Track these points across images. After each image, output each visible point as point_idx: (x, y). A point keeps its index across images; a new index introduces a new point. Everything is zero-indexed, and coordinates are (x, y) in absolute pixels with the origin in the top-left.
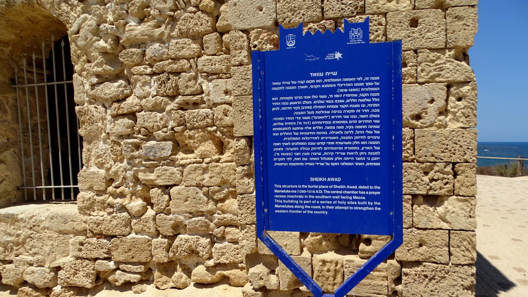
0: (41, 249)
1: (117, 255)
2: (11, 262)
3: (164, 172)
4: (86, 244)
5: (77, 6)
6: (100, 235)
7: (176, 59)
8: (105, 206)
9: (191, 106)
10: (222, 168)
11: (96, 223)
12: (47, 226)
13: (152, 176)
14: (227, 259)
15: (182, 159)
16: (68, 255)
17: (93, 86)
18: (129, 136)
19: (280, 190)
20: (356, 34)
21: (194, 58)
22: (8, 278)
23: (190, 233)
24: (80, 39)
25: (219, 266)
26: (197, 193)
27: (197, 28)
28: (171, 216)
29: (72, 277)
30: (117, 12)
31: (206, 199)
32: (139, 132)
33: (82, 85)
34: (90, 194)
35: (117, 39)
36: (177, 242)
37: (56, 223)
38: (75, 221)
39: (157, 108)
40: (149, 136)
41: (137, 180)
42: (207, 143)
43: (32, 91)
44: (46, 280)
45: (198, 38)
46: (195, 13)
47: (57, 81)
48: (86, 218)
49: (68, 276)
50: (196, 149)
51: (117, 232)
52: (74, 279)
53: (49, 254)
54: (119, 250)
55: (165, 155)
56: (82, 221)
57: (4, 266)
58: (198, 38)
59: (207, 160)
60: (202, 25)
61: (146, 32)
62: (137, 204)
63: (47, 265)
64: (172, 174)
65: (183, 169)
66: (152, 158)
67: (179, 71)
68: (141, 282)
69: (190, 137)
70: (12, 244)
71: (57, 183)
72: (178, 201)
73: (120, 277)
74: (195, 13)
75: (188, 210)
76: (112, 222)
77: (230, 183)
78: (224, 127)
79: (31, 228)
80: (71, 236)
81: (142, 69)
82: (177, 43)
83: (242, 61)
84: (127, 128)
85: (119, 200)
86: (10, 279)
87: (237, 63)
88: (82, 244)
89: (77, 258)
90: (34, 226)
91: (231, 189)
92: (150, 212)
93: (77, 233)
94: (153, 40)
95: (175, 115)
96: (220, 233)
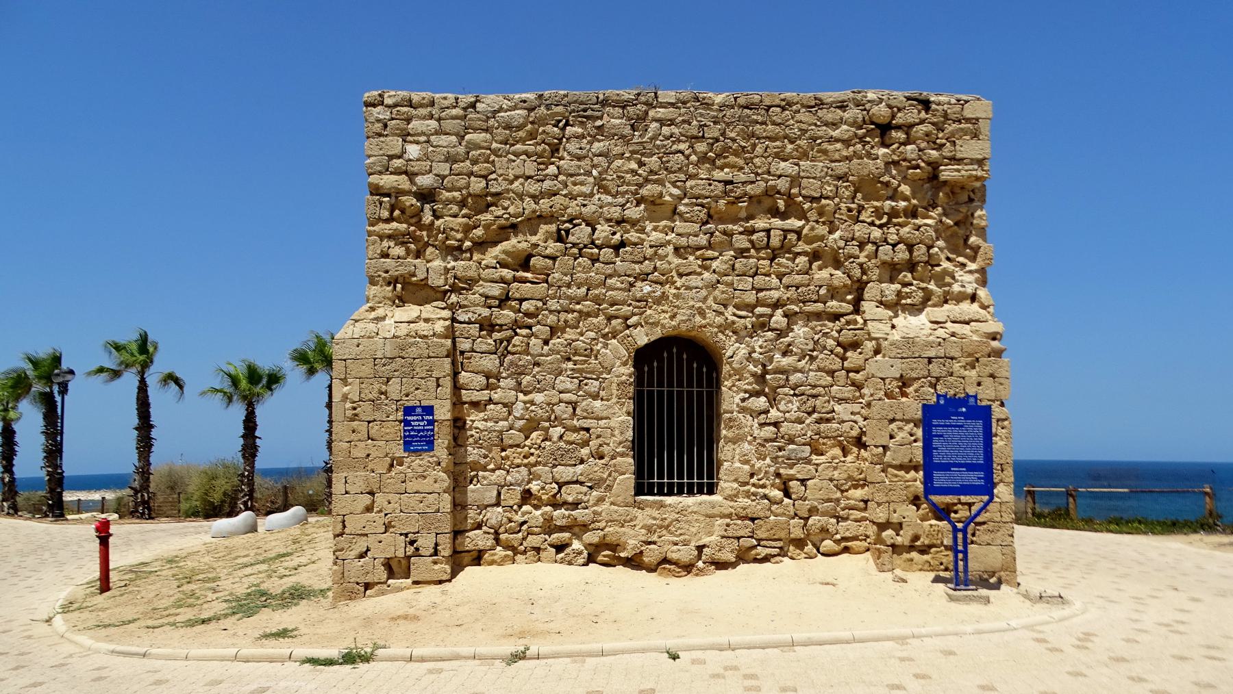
7: (815, 386)
13: (792, 472)
18: (774, 440)
19: (936, 474)
20: (972, 400)
40: (791, 441)
41: (778, 475)
73: (762, 552)
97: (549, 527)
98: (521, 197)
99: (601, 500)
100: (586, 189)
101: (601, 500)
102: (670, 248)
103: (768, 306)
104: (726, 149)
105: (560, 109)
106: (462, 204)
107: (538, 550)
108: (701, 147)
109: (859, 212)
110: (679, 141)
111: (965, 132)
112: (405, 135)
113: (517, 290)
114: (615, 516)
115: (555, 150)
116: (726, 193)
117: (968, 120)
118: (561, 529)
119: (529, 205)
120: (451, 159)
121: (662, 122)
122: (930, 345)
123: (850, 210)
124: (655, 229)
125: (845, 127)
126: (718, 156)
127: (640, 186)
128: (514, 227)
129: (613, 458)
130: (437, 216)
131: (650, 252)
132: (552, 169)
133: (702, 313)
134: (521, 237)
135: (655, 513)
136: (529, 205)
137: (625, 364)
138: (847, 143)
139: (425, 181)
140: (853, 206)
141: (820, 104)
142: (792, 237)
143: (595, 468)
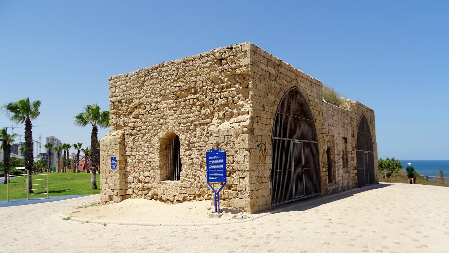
1: (188, 193)
6: (185, 188)
7: (201, 147)
13: (196, 174)
18: (191, 164)
19: (210, 175)
20: (220, 150)
33: (182, 151)
34: (183, 178)
35: (190, 141)
39: (197, 158)
40: (196, 164)
41: (193, 175)
43: (170, 150)
58: (205, 142)
62: (193, 180)
68: (193, 199)
71: (175, 175)
73: (189, 198)
92: (196, 182)
95: (201, 160)
97: (143, 189)
98: (136, 99)
99: (153, 182)
100: (149, 94)
101: (153, 182)
102: (167, 108)
103: (190, 123)
104: (179, 76)
105: (143, 73)
106: (126, 102)
107: (141, 195)
108: (173, 77)
109: (213, 89)
110: (169, 76)
111: (242, 56)
112: (116, 87)
113: (137, 124)
114: (156, 186)
115: (143, 84)
116: (180, 90)
117: (243, 52)
118: (145, 190)
119: (138, 101)
120: (123, 91)
121: (165, 72)
122: (224, 131)
123: (210, 89)
124: (165, 103)
125: (208, 63)
126: (178, 79)
127: (161, 91)
128: (136, 107)
129: (156, 170)
130: (122, 107)
131: (163, 110)
132: (143, 90)
133: (175, 127)
134: (137, 110)
135: (165, 186)
136: (138, 101)
137: (158, 143)
138: (209, 67)
139: (119, 98)
140: (211, 88)
141: (202, 57)
142: (196, 100)
143: (151, 173)
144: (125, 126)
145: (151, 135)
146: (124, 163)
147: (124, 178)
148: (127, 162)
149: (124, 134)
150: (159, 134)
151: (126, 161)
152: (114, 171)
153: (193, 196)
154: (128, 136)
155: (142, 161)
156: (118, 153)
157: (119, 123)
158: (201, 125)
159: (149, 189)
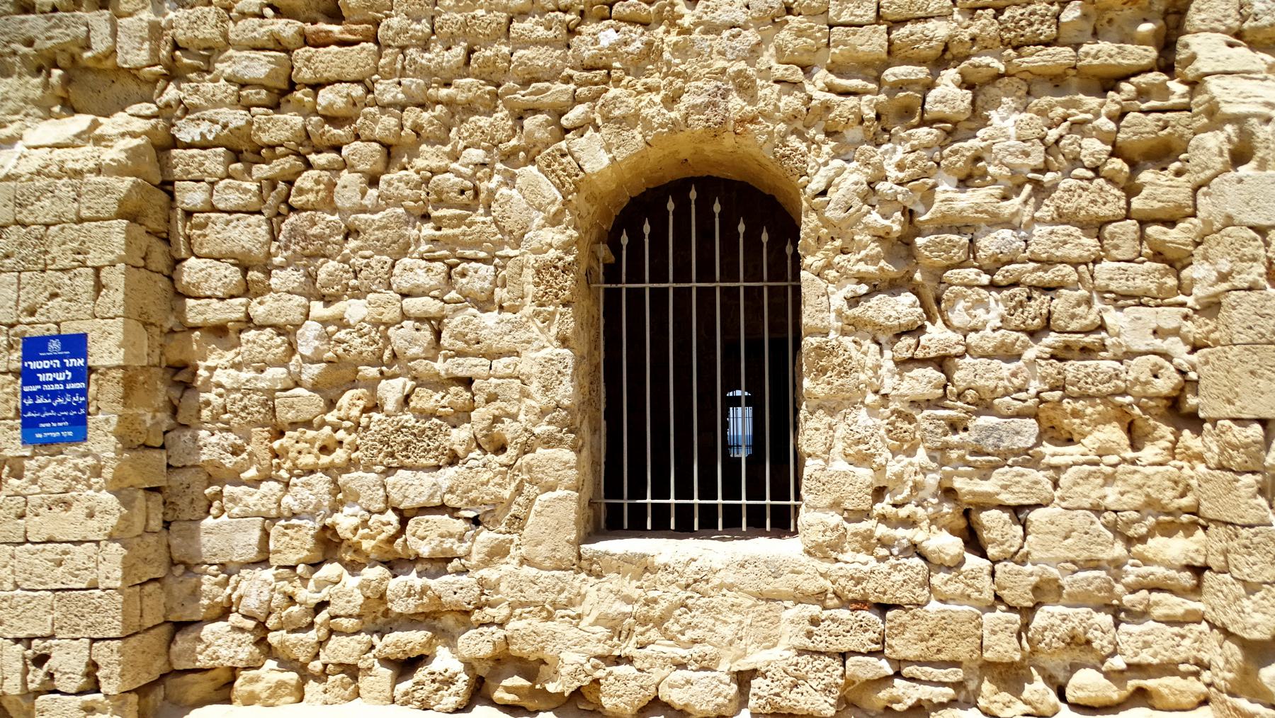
0: (711, 630)
2: (629, 660)
3: (1018, 479)
4: (827, 623)
5: (823, 142)
7: (1048, 263)
8: (868, 543)
9: (1077, 353)
10: (1148, 477)
11: (852, 578)
12: (729, 580)
14: (1154, 656)
15: (1054, 455)
16: (774, 645)
17: (854, 301)
21: (1086, 264)
22: (619, 697)
23: (1069, 602)
24: (831, 205)
25: (1137, 669)
26: (1092, 523)
27: (1095, 209)
28: (1029, 568)
29: (786, 692)
30: (920, 163)
31: (1110, 535)
32: (960, 396)
35: (910, 214)
36: (1040, 619)
37: (753, 576)
38: (799, 573)
39: (1009, 354)
40: (984, 405)
41: (949, 493)
42: (1108, 428)
44: (720, 700)
45: (1096, 227)
46: (1090, 180)
47: (769, 280)
48: (824, 566)
49: (777, 690)
50: (1084, 436)
51: (904, 596)
52: (793, 696)
53: (731, 643)
54: (907, 635)
55: (1022, 445)
56: (814, 574)
57: (608, 669)
58: (1096, 227)
59: (1114, 459)
60: (1105, 204)
61: (986, 207)
63: (724, 666)
64: (1036, 483)
65: (1059, 475)
66: (990, 450)
67: (1053, 285)
69: (1075, 414)
70: (632, 620)
72: (1050, 537)
74: (1090, 180)
75: (1072, 556)
76: (895, 578)
77: (1163, 507)
78: (1151, 398)
79: (688, 586)
80: (788, 604)
81: (973, 276)
82: (1052, 233)
83: (1255, 282)
84: (936, 387)
85: (900, 533)
86: (625, 699)
87: (1246, 285)
88: (815, 622)
89: (802, 652)
90: (695, 581)
91: (1162, 518)
93: (801, 598)
94: (997, 222)
96: (1141, 603)
97: (378, 617)
99: (497, 553)
107: (352, 671)
114: (531, 593)
129: (526, 449)
133: (745, 87)
135: (630, 588)
137: (554, 221)
143: (482, 476)
144: (174, 74)
145: (476, 155)
146: (162, 393)
147: (156, 524)
148: (187, 386)
149: (165, 145)
150: (574, 142)
151: (181, 377)
152: (52, 470)
153: (954, 675)
154: (214, 161)
155: (373, 372)
156: (115, 297)
157: (100, 44)
158: (1034, 84)
159: (432, 618)
